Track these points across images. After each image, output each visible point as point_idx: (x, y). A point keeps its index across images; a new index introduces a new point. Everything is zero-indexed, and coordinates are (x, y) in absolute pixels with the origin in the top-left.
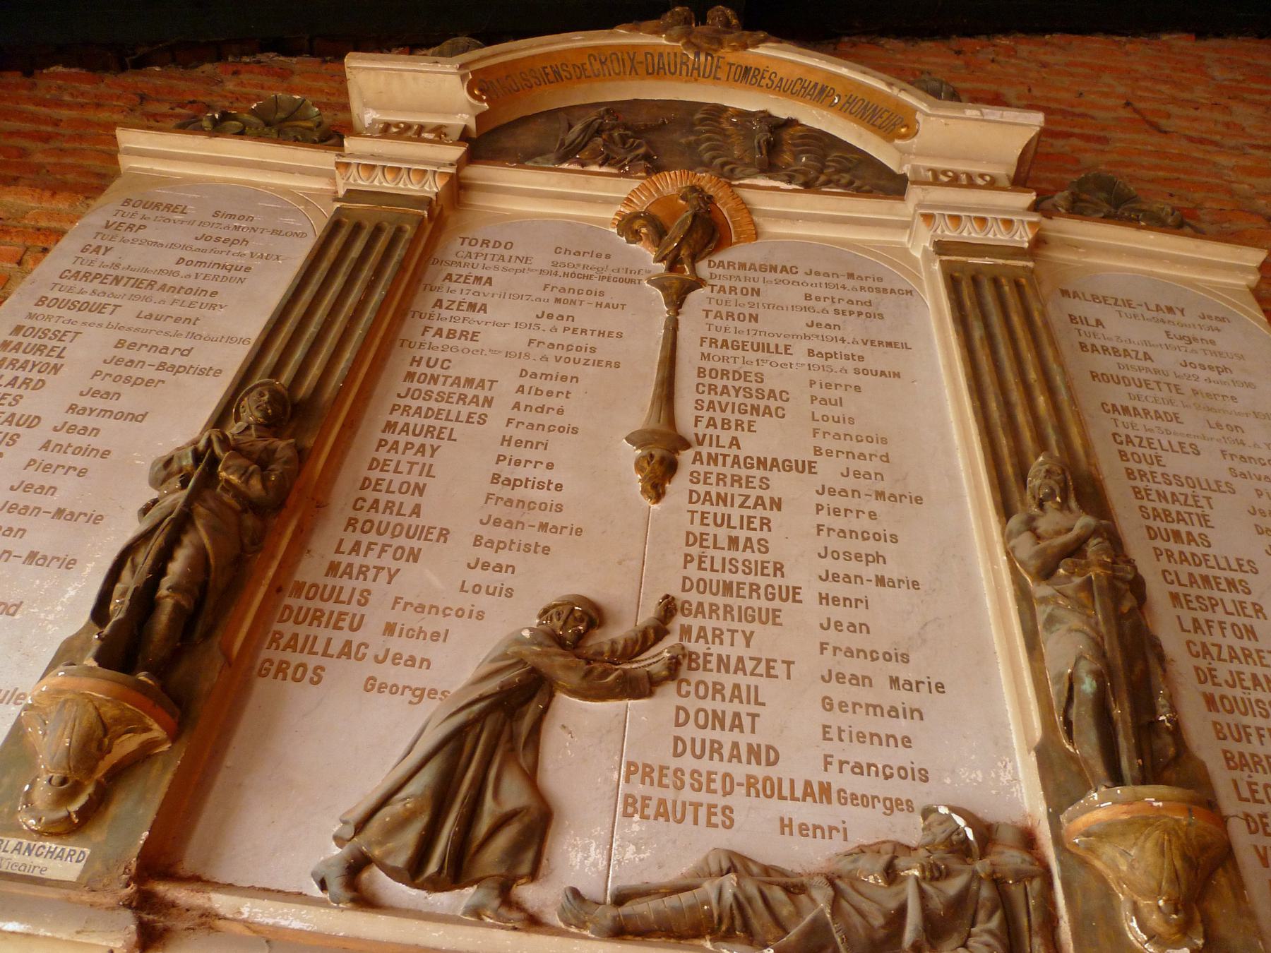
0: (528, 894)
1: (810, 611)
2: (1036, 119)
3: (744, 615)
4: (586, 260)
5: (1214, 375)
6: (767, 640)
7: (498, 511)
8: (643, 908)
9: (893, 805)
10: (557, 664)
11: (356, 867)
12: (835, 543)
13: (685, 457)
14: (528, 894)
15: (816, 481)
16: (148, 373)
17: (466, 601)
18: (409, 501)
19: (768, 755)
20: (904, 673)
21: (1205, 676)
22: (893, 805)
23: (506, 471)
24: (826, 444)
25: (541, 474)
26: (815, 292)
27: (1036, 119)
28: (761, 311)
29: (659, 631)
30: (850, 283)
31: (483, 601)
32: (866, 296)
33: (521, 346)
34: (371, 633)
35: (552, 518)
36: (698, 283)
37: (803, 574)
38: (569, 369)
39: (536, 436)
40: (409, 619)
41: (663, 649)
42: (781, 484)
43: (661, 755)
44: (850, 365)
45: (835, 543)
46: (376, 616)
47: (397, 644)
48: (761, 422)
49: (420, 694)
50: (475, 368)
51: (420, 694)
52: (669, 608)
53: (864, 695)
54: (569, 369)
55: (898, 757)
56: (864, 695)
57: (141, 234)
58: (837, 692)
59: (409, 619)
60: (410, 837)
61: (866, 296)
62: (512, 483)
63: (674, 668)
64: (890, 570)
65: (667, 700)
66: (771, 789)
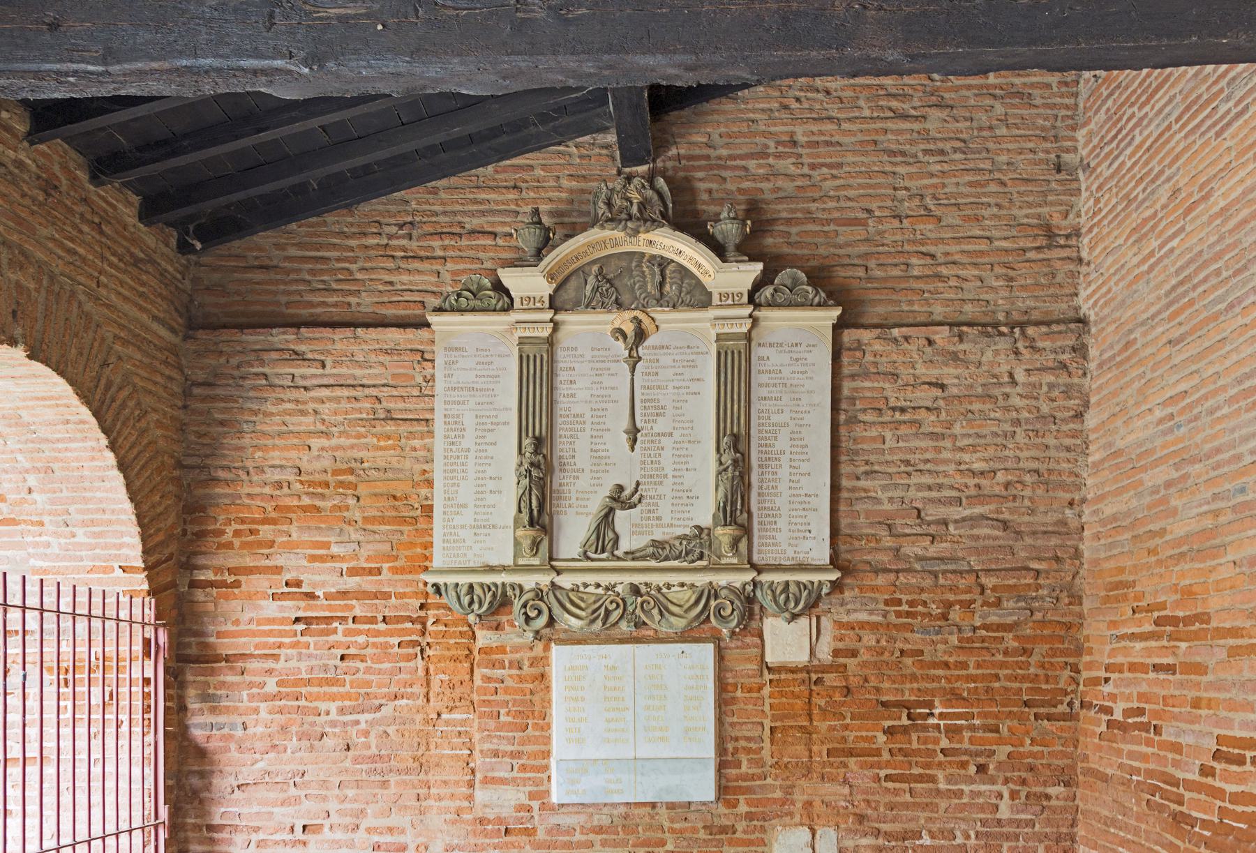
0: (616, 552)
1: (670, 480)
2: (759, 266)
3: (655, 484)
4: (601, 353)
5: (800, 376)
6: (661, 490)
7: (595, 461)
8: (637, 555)
9: (685, 526)
10: (614, 505)
11: (585, 552)
12: (677, 460)
13: (639, 435)
14: (616, 552)
15: (672, 439)
16: (490, 427)
17: (591, 489)
18: (572, 461)
19: (659, 518)
20: (690, 494)
21: (760, 487)
22: (685, 526)
23: (594, 447)
24: (677, 425)
25: (602, 447)
26: (677, 358)
27: (759, 266)
28: (660, 371)
29: (636, 490)
30: (689, 351)
31: (597, 488)
32: (692, 357)
33: (589, 398)
34: (573, 501)
35: (607, 461)
36: (640, 359)
37: (669, 471)
38: (603, 405)
39: (599, 433)
40: (581, 496)
41: (637, 496)
42: (665, 441)
43: (638, 521)
44: (685, 391)
45: (677, 460)
46: (573, 495)
47: (580, 502)
48: (660, 419)
49: (588, 514)
50: (577, 409)
51: (588, 514)
52: (638, 484)
53: (680, 501)
54: (603, 405)
55: (687, 515)
56: (680, 501)
57: (458, 365)
58: (675, 501)
59: (581, 496)
60: (594, 548)
61: (692, 357)
62: (596, 451)
63: (640, 501)
64: (689, 466)
65: (639, 507)
66: (660, 526)
